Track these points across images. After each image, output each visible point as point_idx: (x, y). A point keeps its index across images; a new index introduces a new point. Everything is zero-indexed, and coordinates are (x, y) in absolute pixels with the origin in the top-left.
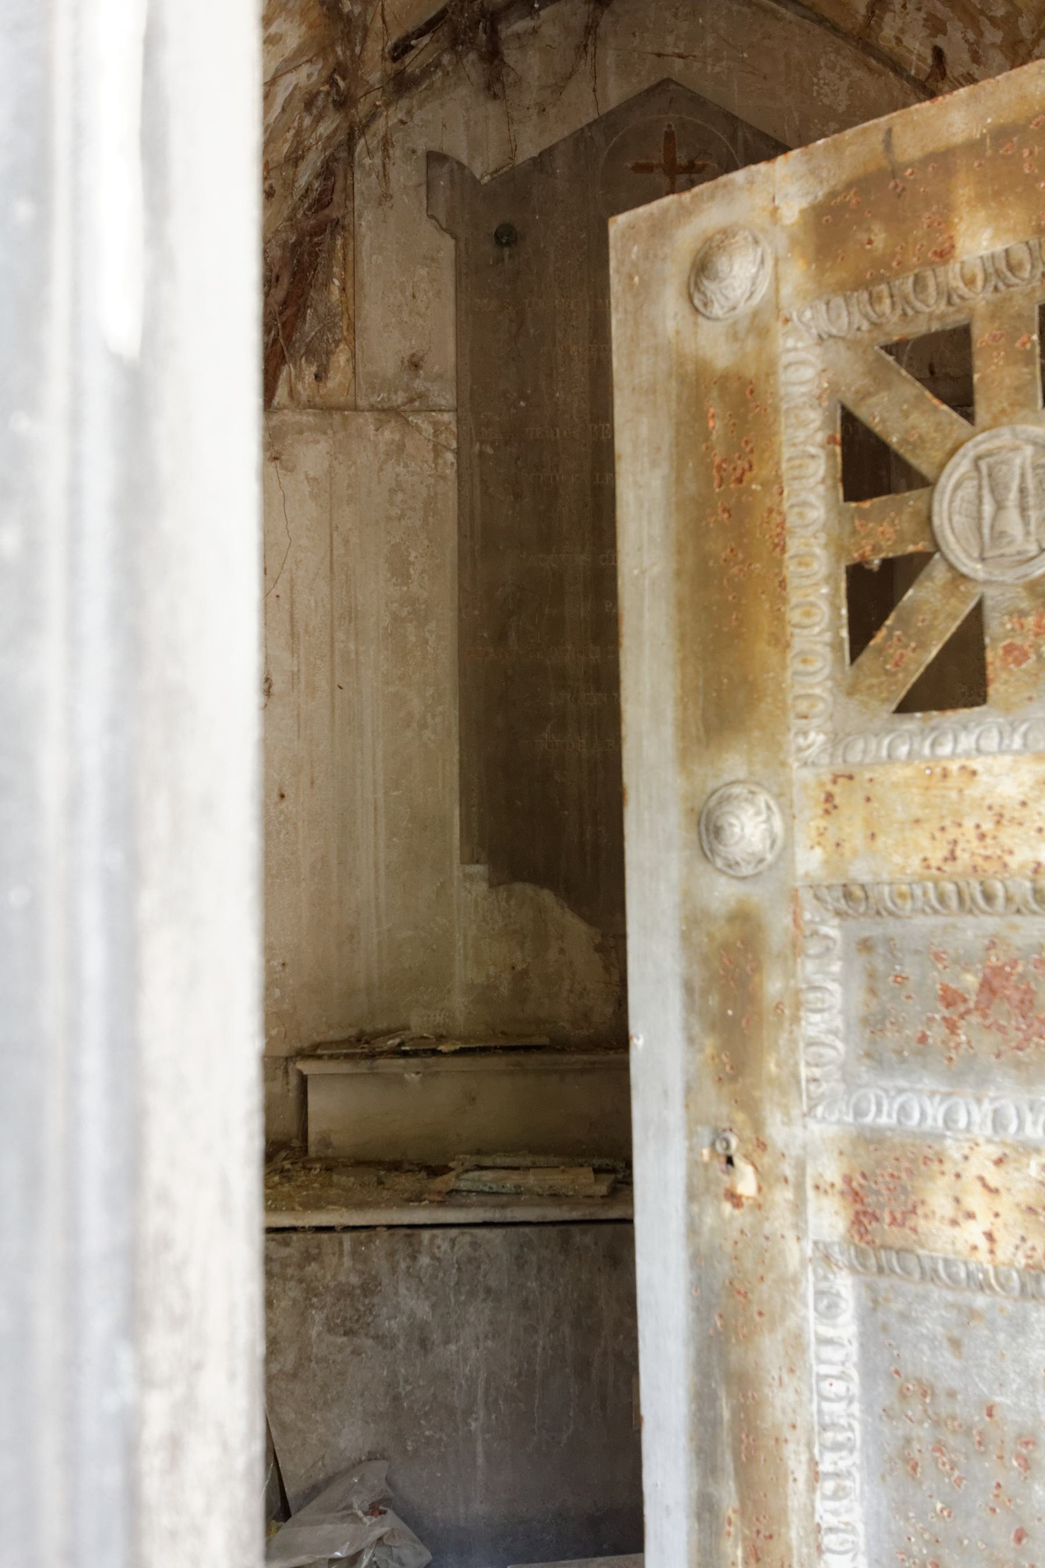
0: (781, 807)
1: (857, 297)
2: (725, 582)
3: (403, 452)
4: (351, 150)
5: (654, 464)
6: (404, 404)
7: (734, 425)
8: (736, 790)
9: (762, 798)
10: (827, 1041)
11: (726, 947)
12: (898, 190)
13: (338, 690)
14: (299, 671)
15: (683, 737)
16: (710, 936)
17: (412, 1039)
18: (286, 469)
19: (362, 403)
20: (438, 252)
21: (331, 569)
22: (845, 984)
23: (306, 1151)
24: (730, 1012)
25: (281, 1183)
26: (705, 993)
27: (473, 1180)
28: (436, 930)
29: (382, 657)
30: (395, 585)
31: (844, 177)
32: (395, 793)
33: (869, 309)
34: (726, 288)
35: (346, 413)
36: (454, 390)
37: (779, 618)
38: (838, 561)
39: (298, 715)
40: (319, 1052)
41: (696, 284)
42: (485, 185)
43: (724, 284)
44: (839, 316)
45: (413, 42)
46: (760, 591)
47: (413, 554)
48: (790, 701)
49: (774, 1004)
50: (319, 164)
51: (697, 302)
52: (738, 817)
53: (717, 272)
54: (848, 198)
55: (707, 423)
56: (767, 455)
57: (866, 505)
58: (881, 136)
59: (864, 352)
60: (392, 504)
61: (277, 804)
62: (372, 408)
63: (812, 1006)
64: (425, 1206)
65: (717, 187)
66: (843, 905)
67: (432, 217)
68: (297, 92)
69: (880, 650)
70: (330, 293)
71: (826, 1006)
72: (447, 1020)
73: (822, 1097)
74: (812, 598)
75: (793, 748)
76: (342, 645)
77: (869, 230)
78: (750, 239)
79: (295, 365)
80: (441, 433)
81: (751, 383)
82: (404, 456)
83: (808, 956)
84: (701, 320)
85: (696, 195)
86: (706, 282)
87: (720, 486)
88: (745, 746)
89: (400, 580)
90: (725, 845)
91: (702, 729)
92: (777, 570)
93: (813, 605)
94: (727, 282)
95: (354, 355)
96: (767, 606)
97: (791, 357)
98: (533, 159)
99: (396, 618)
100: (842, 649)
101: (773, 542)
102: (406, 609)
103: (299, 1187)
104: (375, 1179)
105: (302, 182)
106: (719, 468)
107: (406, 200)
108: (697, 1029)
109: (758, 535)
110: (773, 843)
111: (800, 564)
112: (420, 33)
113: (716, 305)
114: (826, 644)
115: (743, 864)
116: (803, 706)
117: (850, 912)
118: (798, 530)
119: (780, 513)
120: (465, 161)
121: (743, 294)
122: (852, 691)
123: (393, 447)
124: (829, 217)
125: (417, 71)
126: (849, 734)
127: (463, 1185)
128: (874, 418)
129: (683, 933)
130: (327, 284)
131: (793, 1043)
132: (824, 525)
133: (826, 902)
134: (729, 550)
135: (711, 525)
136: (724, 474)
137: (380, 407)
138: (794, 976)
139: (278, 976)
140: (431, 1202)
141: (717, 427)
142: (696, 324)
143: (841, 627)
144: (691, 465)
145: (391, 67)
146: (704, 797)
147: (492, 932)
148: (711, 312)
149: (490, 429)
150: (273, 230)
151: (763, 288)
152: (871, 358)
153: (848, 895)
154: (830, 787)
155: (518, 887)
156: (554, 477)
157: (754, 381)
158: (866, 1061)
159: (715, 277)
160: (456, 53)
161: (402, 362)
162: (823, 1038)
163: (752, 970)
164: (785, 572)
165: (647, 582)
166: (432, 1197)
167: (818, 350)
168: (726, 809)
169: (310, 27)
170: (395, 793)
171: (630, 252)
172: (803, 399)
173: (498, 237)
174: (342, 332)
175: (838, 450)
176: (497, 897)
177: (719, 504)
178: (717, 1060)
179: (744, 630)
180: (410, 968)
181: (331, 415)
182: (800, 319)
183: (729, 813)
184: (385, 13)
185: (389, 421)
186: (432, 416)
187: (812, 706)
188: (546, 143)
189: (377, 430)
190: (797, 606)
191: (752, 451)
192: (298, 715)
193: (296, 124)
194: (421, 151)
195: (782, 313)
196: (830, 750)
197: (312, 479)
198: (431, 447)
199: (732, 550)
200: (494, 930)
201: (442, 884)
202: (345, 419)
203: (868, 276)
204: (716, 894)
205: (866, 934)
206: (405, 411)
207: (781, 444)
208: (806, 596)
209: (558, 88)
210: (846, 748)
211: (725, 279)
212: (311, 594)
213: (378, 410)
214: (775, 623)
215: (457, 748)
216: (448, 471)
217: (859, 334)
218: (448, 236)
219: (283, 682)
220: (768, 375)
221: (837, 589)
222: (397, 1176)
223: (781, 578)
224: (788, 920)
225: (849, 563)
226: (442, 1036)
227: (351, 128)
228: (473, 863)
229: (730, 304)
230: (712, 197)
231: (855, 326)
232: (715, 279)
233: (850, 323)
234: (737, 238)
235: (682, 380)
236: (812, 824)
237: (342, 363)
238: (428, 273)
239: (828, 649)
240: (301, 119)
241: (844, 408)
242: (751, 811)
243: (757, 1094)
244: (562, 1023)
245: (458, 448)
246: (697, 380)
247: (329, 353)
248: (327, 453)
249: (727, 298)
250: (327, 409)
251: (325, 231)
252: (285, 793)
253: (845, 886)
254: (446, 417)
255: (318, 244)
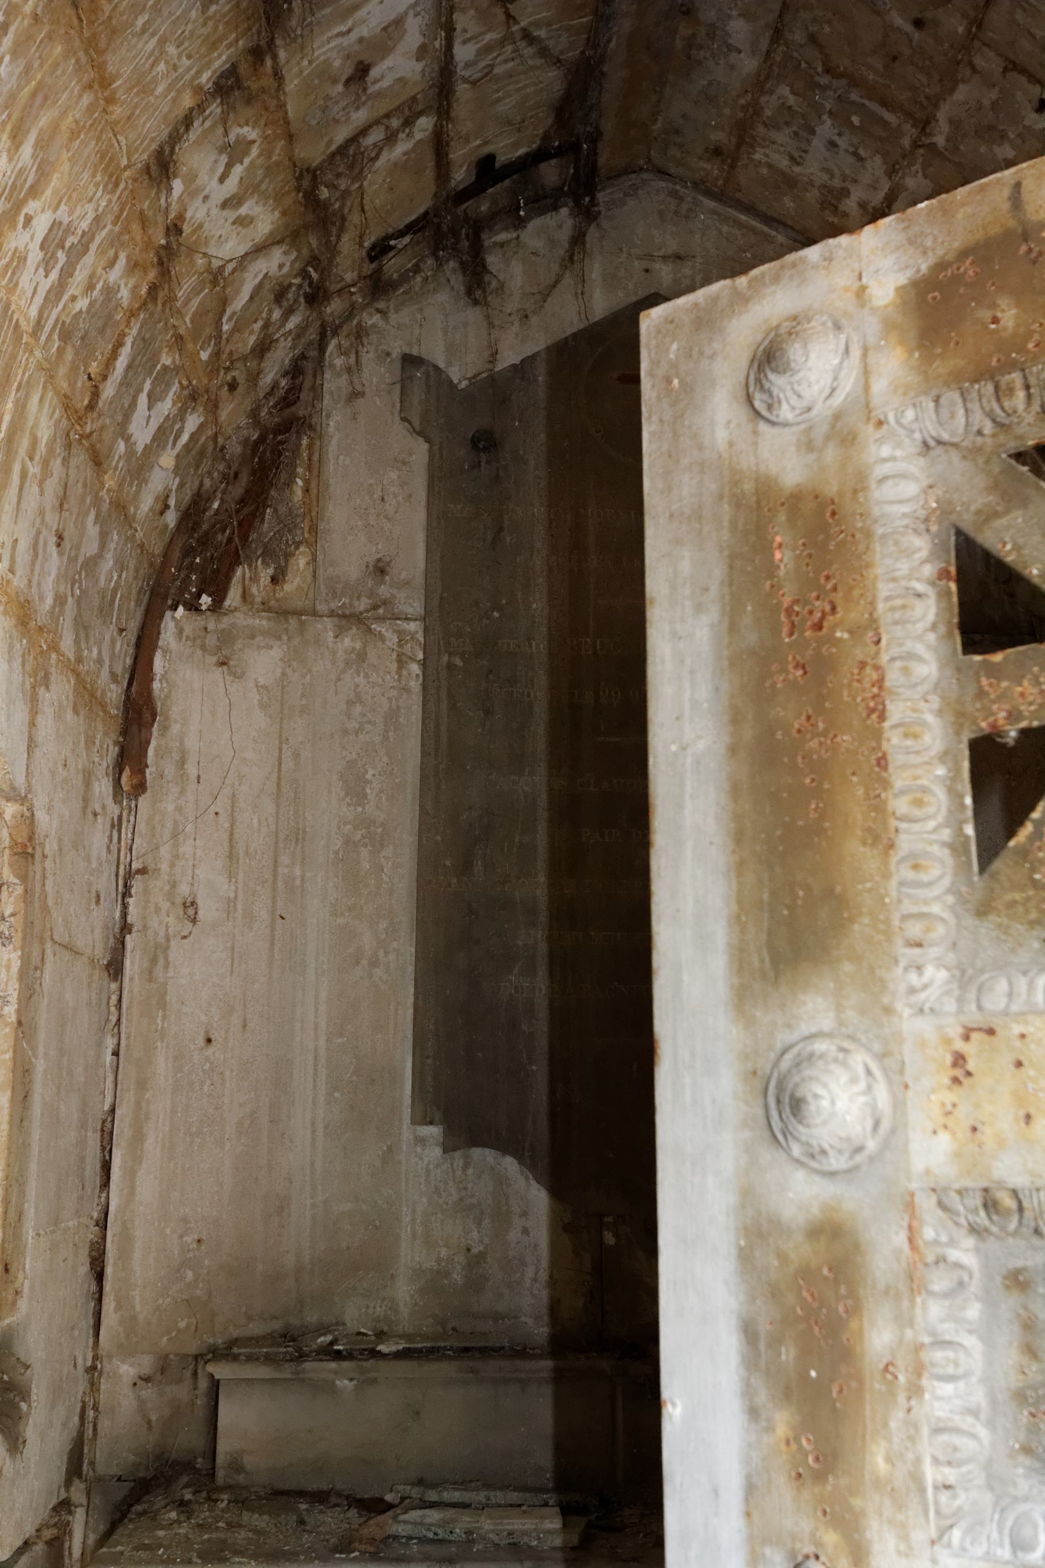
0: (885, 1071)
1: (979, 391)
2: (800, 760)
3: (364, 661)
4: (322, 348)
5: (699, 608)
6: (367, 611)
7: (810, 556)
8: (820, 1046)
9: (859, 1059)
10: (964, 1426)
11: (806, 1274)
12: (1033, 255)
13: (280, 921)
14: (236, 898)
15: (740, 970)
16: (782, 1257)
17: (347, 1335)
18: (234, 674)
19: (321, 608)
20: (411, 455)
21: (279, 785)
22: (987, 1341)
23: (213, 1475)
24: (813, 1374)
25: (178, 1522)
26: (775, 1341)
27: (415, 1524)
28: (380, 1202)
29: (331, 884)
30: (349, 805)
31: (956, 244)
32: (340, 1040)
33: (995, 406)
34: (799, 382)
35: (303, 618)
36: (423, 599)
37: (878, 808)
38: (958, 733)
39: (233, 948)
40: (235, 1350)
41: (758, 381)
42: (463, 389)
43: (797, 377)
44: (953, 416)
45: (392, 243)
46: (849, 771)
47: (371, 772)
48: (896, 923)
49: (881, 1366)
50: (287, 362)
51: (757, 404)
52: (825, 1086)
53: (788, 363)
54: (962, 270)
55: (773, 555)
56: (856, 593)
57: (998, 657)
58: (1006, 192)
59: (987, 462)
60: (349, 716)
61: (202, 1049)
62: (332, 614)
63: (940, 1371)
64: (355, 1559)
65: (782, 267)
66: (982, 1216)
67: (404, 419)
68: (267, 282)
69: (1024, 853)
70: (292, 493)
71: (960, 1371)
72: (389, 1312)
73: (958, 1514)
74: (924, 782)
75: (902, 988)
76: (286, 871)
77: (994, 306)
78: (829, 324)
79: (250, 566)
80: (407, 642)
81: (833, 502)
82: (365, 665)
83: (931, 1293)
84: (763, 426)
85: (756, 278)
86: (772, 376)
87: (791, 634)
88: (832, 985)
89: (354, 800)
90: (808, 1126)
91: (767, 959)
92: (874, 744)
93: (925, 790)
94: (801, 374)
95: (314, 559)
96: (860, 792)
97: (886, 469)
98: (514, 366)
99: (348, 841)
100: (966, 851)
101: (868, 707)
102: (360, 832)
103: (200, 1526)
104: (295, 1517)
105: (267, 379)
106: (789, 611)
107: (378, 403)
108: (762, 1397)
109: (846, 698)
110: (876, 1125)
111: (906, 735)
112: (400, 234)
113: (785, 406)
114: (944, 844)
115: (831, 1152)
116: (915, 930)
117: (994, 1229)
118: (901, 690)
119: (877, 668)
120: (442, 365)
121: (821, 392)
122: (983, 910)
123: (353, 656)
124: (936, 294)
125: (395, 276)
126: (982, 971)
127: (401, 1529)
128: (1005, 544)
129: (741, 1249)
130: (289, 483)
131: (912, 1427)
132: (936, 686)
133: (958, 1214)
134: (804, 717)
135: (779, 686)
136: (796, 619)
137: (340, 612)
138: (911, 1323)
139: (191, 1255)
140: (362, 1553)
141: (785, 560)
142: (755, 433)
143: (965, 821)
144: (749, 608)
145: (368, 268)
146: (772, 1056)
147: (445, 1207)
148: (778, 416)
149: (461, 640)
150: (234, 426)
151: (848, 383)
152: (997, 469)
153: (990, 1205)
154: (959, 1045)
155: (476, 1152)
156: (529, 694)
157: (836, 500)
158: (1022, 1458)
159: (785, 369)
160: (437, 258)
161: (367, 566)
162: (958, 1420)
163: (847, 1311)
164: (885, 745)
165: (689, 760)
166: (363, 1548)
167: (922, 462)
168: (807, 1073)
169: (284, 214)
170: (340, 1040)
171: (668, 350)
172: (905, 522)
173: (474, 442)
174: (303, 533)
175: (953, 586)
176: (452, 1165)
177: (790, 658)
178: (794, 1447)
179: (827, 825)
180: (348, 1248)
181: (287, 621)
182: (898, 422)
183: (811, 1078)
184: (365, 202)
185: (351, 628)
186: (397, 625)
187: (928, 930)
188: (529, 349)
189: (336, 637)
190: (903, 792)
191: (835, 589)
192: (233, 948)
193: (264, 315)
194: (396, 353)
195: (873, 414)
196: (957, 993)
197: (262, 686)
198: (394, 656)
199: (809, 718)
200: (447, 1204)
201: (390, 1148)
202: (302, 623)
203: (994, 363)
204: (791, 1195)
205: (1019, 1263)
206: (369, 618)
207: (876, 578)
208: (916, 778)
209: (546, 293)
210: (980, 989)
211: (798, 371)
212: (255, 813)
213: (338, 615)
214: (873, 814)
215: (412, 990)
216: (412, 684)
217: (979, 439)
218: (421, 440)
219: (217, 910)
220: (856, 492)
221: (958, 770)
222: (321, 1512)
223: (880, 755)
224: (901, 1239)
225: (973, 736)
226: (382, 1332)
227: (323, 327)
228: (426, 1124)
229: (805, 403)
230: (776, 279)
231: (975, 428)
232: (785, 372)
233: (967, 424)
234: (813, 324)
235: (737, 503)
236: (933, 1097)
237: (302, 566)
238: (399, 477)
239: (947, 851)
240: (270, 311)
241: (959, 532)
242: (844, 1078)
243: (857, 1502)
244: (523, 1319)
245: (425, 659)
246: (758, 502)
247: (288, 556)
248: (281, 660)
249: (799, 396)
250: (283, 613)
251: (290, 429)
252: (213, 1037)
253: (986, 1190)
254: (413, 626)
255: (282, 443)
